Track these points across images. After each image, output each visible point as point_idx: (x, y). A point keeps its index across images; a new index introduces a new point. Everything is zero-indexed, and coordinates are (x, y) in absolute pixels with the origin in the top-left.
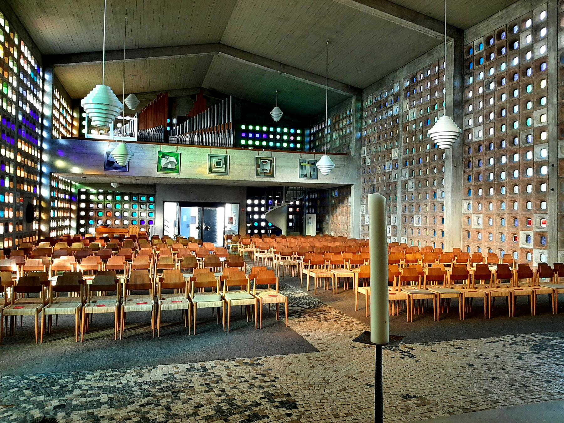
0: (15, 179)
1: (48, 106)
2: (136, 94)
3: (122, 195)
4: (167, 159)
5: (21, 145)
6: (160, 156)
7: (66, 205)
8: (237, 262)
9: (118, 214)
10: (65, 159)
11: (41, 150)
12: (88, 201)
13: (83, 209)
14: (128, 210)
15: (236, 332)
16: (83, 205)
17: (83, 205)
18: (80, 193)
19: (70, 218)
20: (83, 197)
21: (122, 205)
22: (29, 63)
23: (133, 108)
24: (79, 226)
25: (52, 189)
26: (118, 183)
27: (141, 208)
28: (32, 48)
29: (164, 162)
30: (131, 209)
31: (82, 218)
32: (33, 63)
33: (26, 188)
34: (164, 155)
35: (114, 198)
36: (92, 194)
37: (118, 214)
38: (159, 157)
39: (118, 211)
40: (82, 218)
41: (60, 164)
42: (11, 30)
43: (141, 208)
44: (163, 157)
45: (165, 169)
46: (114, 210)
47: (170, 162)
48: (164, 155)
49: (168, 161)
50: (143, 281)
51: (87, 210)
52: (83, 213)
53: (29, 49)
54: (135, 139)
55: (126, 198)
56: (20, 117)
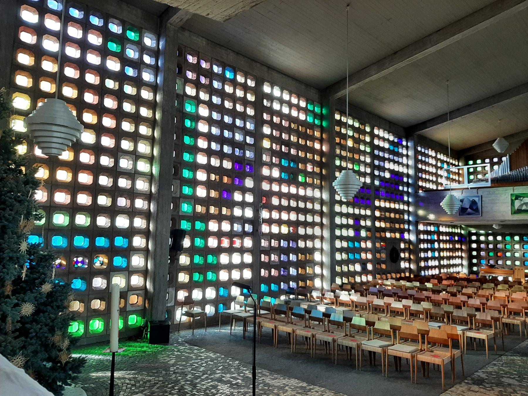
0: (372, 230)
1: (412, 167)
2: (506, 137)
3: (512, 236)
4: (521, 200)
5: (377, 203)
6: (514, 198)
7: (448, 246)
8: (484, 319)
9: (508, 254)
10: (426, 209)
11: (408, 204)
12: (478, 242)
13: (474, 250)
14: (519, 250)
15: (392, 379)
16: (474, 246)
17: (474, 246)
18: (471, 234)
19: (462, 258)
20: (474, 238)
21: (512, 246)
22: (384, 139)
23: (501, 150)
24: (471, 265)
25: (418, 233)
26: (499, 225)
27: (523, 248)
28: (390, 127)
29: (517, 204)
30: (522, 249)
31: (474, 257)
32: (391, 138)
33: (388, 235)
34: (517, 197)
35: (495, 238)
36: (482, 235)
37: (508, 254)
38: (512, 200)
39: (508, 251)
40: (474, 257)
41: (421, 212)
42: (361, 123)
43: (523, 248)
44: (517, 198)
45: (519, 211)
46: (505, 251)
47: (525, 203)
48: (517, 197)
49: (522, 202)
50: (339, 319)
51: (478, 250)
52: (475, 253)
53: (385, 130)
54: (489, 184)
55: (517, 238)
56: (377, 183)
